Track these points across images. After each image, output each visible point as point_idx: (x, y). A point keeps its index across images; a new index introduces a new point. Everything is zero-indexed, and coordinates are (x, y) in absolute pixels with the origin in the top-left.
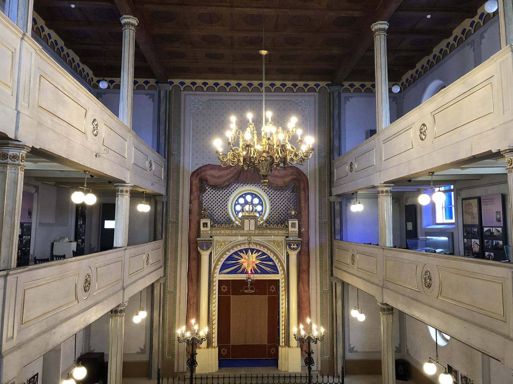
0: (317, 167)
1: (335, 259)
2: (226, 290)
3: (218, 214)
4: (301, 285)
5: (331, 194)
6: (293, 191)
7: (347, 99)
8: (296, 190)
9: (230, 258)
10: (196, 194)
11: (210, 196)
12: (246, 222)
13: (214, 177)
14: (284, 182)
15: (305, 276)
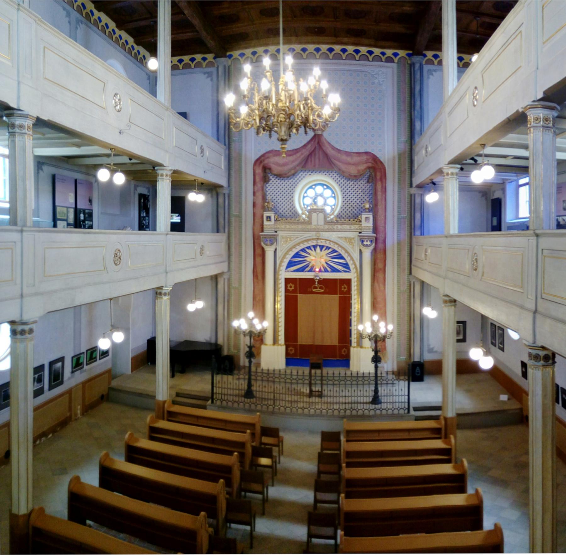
0: (396, 154)
1: (414, 256)
2: (293, 352)
3: (283, 208)
4: (376, 284)
5: (411, 186)
6: (368, 182)
7: (430, 72)
8: (372, 180)
9: (297, 255)
10: (259, 185)
11: (274, 187)
12: (314, 215)
13: (277, 164)
14: (359, 171)
15: (380, 275)
